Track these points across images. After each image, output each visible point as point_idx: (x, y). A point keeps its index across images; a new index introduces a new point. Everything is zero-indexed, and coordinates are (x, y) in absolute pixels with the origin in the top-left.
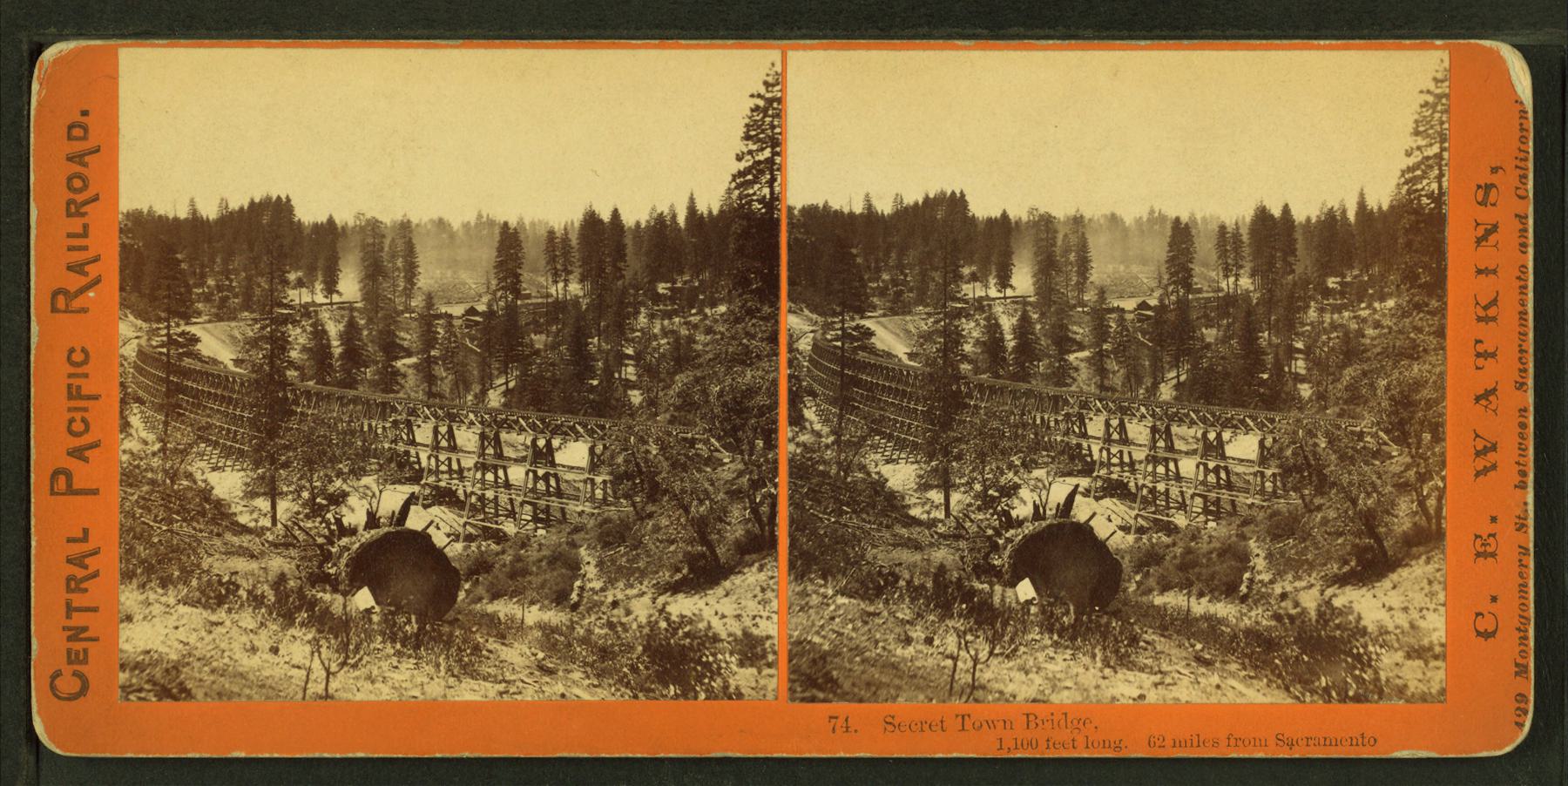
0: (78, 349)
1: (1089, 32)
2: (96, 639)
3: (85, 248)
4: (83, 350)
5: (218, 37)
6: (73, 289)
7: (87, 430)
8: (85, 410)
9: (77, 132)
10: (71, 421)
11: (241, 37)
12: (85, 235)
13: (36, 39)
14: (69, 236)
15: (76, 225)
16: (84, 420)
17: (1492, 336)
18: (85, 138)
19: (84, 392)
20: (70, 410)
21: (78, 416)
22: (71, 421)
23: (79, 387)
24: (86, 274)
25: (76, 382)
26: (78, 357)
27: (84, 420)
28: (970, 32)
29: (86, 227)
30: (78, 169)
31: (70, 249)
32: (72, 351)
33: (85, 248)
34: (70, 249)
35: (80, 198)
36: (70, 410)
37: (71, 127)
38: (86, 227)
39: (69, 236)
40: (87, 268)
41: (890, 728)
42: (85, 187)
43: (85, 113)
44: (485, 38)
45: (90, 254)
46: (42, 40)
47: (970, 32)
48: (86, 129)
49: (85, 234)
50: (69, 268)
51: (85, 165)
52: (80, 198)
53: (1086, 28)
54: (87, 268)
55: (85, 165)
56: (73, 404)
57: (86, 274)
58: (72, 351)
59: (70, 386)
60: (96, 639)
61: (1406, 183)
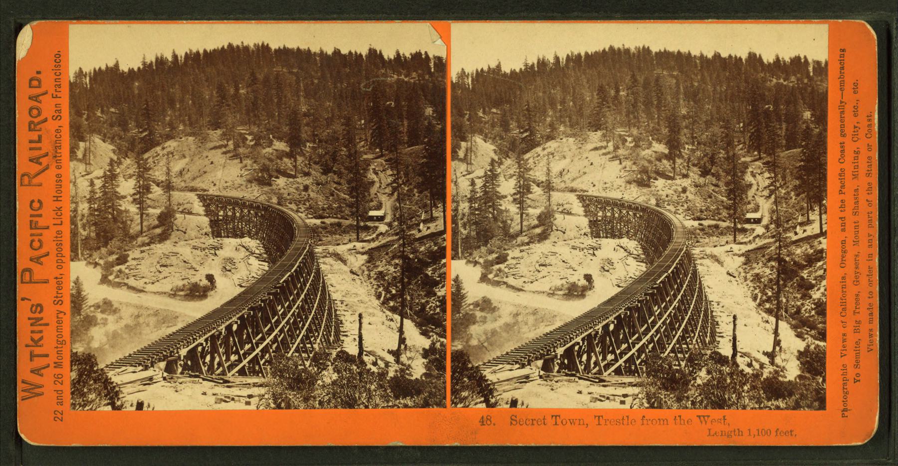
0: (36, 201)
1: (618, 15)
2: (47, 325)
3: (40, 149)
4: (39, 201)
6: (33, 173)
7: (41, 247)
8: (41, 235)
9: (35, 83)
10: (32, 241)
12: (39, 141)
13: (19, 21)
14: (31, 142)
16: (40, 241)
17: (870, 198)
18: (39, 87)
20: (31, 235)
21: (36, 238)
22: (32, 241)
24: (40, 164)
25: (34, 219)
26: (36, 205)
27: (40, 241)
29: (40, 137)
30: (36, 104)
32: (32, 202)
33: (40, 149)
35: (36, 120)
36: (31, 235)
37: (31, 80)
38: (40, 137)
39: (31, 142)
41: (514, 422)
42: (39, 114)
43: (38, 73)
44: (274, 19)
45: (42, 152)
46: (22, 21)
47: (550, 15)
48: (39, 81)
51: (40, 102)
52: (36, 120)
53: (616, 12)
54: (41, 160)
55: (40, 102)
56: (34, 231)
57: (40, 164)
58: (32, 202)
60: (47, 325)
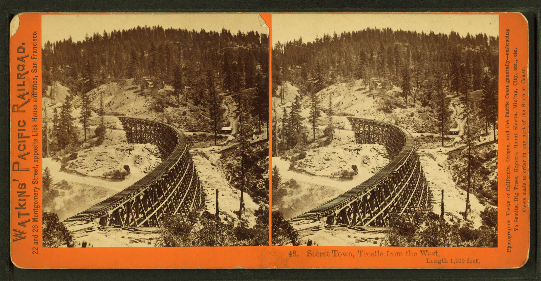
0: (22, 121)
1: (373, 9)
2: (28, 196)
3: (24, 90)
4: (24, 121)
5: (414, 11)
6: (20, 104)
7: (25, 149)
8: (25, 142)
9: (21, 50)
10: (20, 145)
11: (398, 11)
13: (11, 13)
14: (19, 85)
15: (21, 82)
16: (24, 145)
18: (24, 52)
19: (22, 167)
20: (19, 142)
21: (22, 144)
22: (20, 145)
23: (22, 134)
24: (24, 99)
25: (21, 132)
26: (22, 124)
27: (24, 145)
28: (332, 9)
30: (21, 62)
31: (18, 90)
32: (19, 122)
33: (24, 90)
34: (18, 90)
39: (19, 85)
40: (25, 97)
42: (24, 69)
43: (23, 44)
44: (165, 12)
46: (14, 13)
47: (332, 9)
48: (24, 49)
49: (24, 85)
50: (19, 97)
51: (24, 61)
52: (22, 73)
53: (371, 7)
55: (24, 61)
56: (20, 140)
57: (24, 99)
58: (19, 122)
59: (19, 134)
60: (28, 196)
61: (437, 60)
